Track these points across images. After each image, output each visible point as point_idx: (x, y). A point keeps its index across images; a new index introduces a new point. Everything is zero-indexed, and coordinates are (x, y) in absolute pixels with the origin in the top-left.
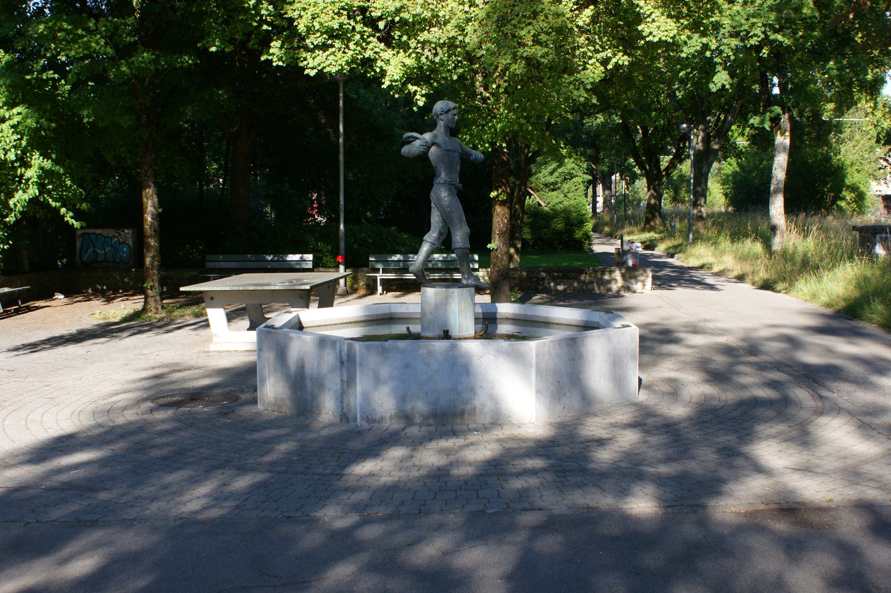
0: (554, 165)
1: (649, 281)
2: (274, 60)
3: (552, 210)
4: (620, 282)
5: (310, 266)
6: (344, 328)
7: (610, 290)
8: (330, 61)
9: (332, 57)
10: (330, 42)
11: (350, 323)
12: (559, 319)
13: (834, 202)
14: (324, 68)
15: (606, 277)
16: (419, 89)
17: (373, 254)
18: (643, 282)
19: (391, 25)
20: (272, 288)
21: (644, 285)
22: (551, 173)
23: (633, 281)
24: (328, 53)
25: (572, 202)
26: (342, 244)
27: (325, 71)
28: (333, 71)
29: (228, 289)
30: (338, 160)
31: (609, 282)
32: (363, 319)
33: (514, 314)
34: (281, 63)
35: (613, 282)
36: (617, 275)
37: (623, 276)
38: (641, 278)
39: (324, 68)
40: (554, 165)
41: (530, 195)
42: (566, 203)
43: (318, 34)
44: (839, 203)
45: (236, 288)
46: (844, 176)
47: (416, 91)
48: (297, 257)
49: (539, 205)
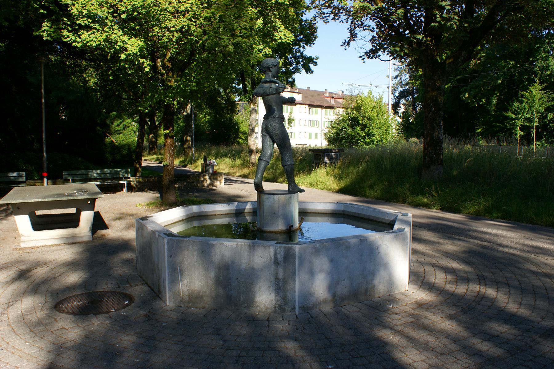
0: (120, 121)
1: (223, 181)
2: (45, 35)
3: (119, 144)
4: (209, 181)
5: (24, 179)
6: (175, 226)
7: (204, 186)
8: (92, 38)
9: (93, 35)
10: (92, 25)
11: (174, 223)
12: (311, 209)
13: (235, 139)
14: (88, 42)
15: (202, 179)
16: (145, 61)
17: (66, 170)
18: (220, 181)
19: (131, 18)
20: (75, 198)
21: (221, 183)
22: (118, 125)
23: (215, 181)
24: (89, 33)
25: (130, 140)
26: (45, 165)
27: (88, 44)
28: (94, 45)
29: (40, 200)
30: (41, 112)
31: (203, 181)
32: (181, 219)
33: (333, 210)
34: (49, 38)
35: (205, 182)
36: (207, 177)
37: (210, 178)
38: (219, 179)
39: (88, 42)
40: (120, 121)
41: (108, 136)
42: (127, 141)
43: (85, 19)
44: (238, 140)
45: (46, 200)
46: (239, 128)
47: (144, 62)
48: (15, 174)
49: (113, 141)
